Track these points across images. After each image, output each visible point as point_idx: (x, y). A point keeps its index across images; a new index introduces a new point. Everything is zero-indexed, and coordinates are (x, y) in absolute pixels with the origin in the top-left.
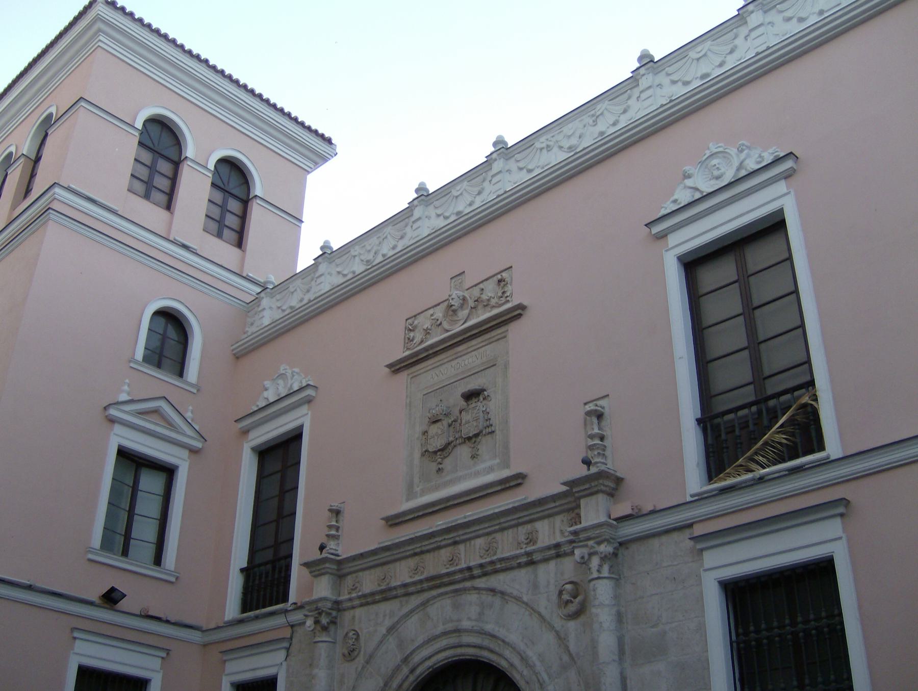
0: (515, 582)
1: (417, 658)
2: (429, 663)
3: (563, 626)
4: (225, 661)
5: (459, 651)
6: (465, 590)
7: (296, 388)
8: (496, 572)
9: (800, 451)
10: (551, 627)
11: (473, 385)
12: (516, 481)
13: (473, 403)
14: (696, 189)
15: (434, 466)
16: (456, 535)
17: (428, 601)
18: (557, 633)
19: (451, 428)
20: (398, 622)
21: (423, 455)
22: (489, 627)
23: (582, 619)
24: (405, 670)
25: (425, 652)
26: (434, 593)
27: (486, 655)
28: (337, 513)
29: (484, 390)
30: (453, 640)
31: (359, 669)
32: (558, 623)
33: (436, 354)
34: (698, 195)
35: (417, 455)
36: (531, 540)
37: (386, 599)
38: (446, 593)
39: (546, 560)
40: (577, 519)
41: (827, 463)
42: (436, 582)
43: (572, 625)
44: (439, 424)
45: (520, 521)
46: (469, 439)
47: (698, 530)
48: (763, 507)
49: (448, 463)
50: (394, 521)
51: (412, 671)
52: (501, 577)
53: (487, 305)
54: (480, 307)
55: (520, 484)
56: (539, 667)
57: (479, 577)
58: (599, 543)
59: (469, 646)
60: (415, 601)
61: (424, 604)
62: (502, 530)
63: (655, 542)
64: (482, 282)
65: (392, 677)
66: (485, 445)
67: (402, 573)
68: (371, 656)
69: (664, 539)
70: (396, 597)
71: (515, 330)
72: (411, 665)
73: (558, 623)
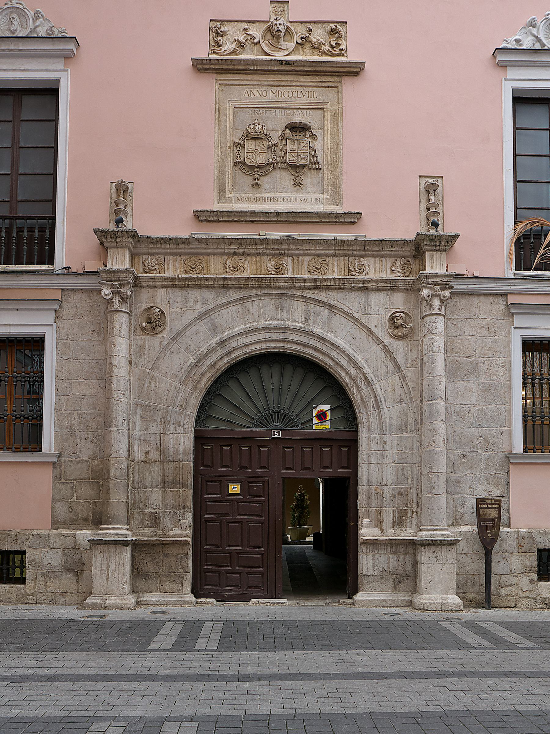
0: (350, 301)
1: (234, 344)
2: (247, 350)
3: (391, 343)
4: (513, 314)
5: (281, 345)
6: (292, 296)
7: (42, 32)
8: (328, 288)
9: (47, 261)
10: (379, 341)
11: (298, 118)
12: (352, 219)
13: (298, 136)
14: (539, 40)
15: (249, 180)
16: (280, 249)
17: (249, 297)
18: (384, 346)
19: (270, 149)
20: (212, 310)
21: (235, 165)
22: (318, 330)
23: (410, 341)
24: (220, 352)
25: (242, 341)
26: (257, 292)
27: (309, 353)
28: (431, 189)
29: (310, 128)
30: (278, 335)
31: (165, 343)
32: (387, 340)
33: (255, 72)
34: (538, 46)
35: (229, 163)
36: (279, 270)
37: (200, 287)
38: (270, 295)
39: (378, 290)
40: (423, 268)
41: (52, 273)
42: (260, 284)
43: (400, 344)
44: (257, 142)
45: (309, 252)
46: (294, 167)
47: (511, 299)
48: (532, 297)
49: (265, 181)
50: (202, 217)
51: (228, 354)
52: (332, 294)
53: (316, 48)
54: (307, 46)
55: (353, 223)
56: (367, 370)
57: (310, 289)
58: (442, 289)
59: (293, 342)
60: (233, 295)
61: (242, 299)
62: (334, 255)
63: (475, 300)
64: (315, 22)
65: (205, 356)
66: (309, 178)
67: (215, 268)
68: (179, 334)
69: (482, 299)
70: (212, 287)
71: (348, 86)
72: (227, 349)
73: (387, 340)
